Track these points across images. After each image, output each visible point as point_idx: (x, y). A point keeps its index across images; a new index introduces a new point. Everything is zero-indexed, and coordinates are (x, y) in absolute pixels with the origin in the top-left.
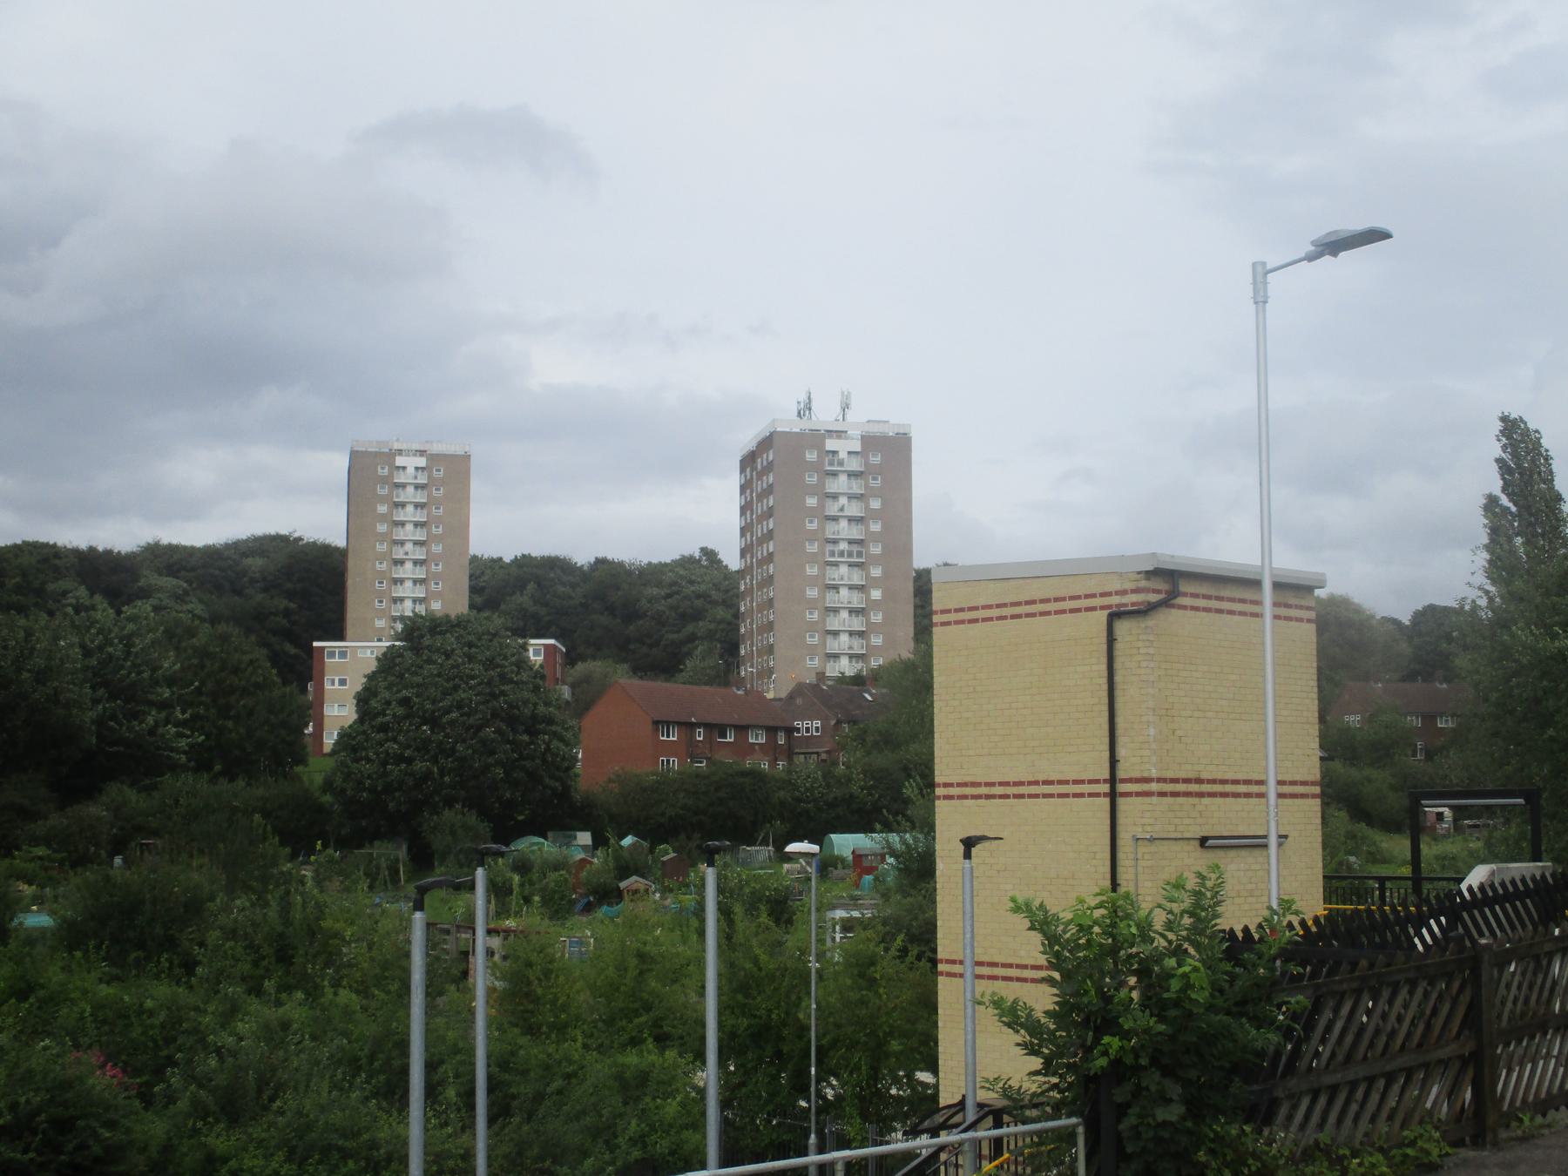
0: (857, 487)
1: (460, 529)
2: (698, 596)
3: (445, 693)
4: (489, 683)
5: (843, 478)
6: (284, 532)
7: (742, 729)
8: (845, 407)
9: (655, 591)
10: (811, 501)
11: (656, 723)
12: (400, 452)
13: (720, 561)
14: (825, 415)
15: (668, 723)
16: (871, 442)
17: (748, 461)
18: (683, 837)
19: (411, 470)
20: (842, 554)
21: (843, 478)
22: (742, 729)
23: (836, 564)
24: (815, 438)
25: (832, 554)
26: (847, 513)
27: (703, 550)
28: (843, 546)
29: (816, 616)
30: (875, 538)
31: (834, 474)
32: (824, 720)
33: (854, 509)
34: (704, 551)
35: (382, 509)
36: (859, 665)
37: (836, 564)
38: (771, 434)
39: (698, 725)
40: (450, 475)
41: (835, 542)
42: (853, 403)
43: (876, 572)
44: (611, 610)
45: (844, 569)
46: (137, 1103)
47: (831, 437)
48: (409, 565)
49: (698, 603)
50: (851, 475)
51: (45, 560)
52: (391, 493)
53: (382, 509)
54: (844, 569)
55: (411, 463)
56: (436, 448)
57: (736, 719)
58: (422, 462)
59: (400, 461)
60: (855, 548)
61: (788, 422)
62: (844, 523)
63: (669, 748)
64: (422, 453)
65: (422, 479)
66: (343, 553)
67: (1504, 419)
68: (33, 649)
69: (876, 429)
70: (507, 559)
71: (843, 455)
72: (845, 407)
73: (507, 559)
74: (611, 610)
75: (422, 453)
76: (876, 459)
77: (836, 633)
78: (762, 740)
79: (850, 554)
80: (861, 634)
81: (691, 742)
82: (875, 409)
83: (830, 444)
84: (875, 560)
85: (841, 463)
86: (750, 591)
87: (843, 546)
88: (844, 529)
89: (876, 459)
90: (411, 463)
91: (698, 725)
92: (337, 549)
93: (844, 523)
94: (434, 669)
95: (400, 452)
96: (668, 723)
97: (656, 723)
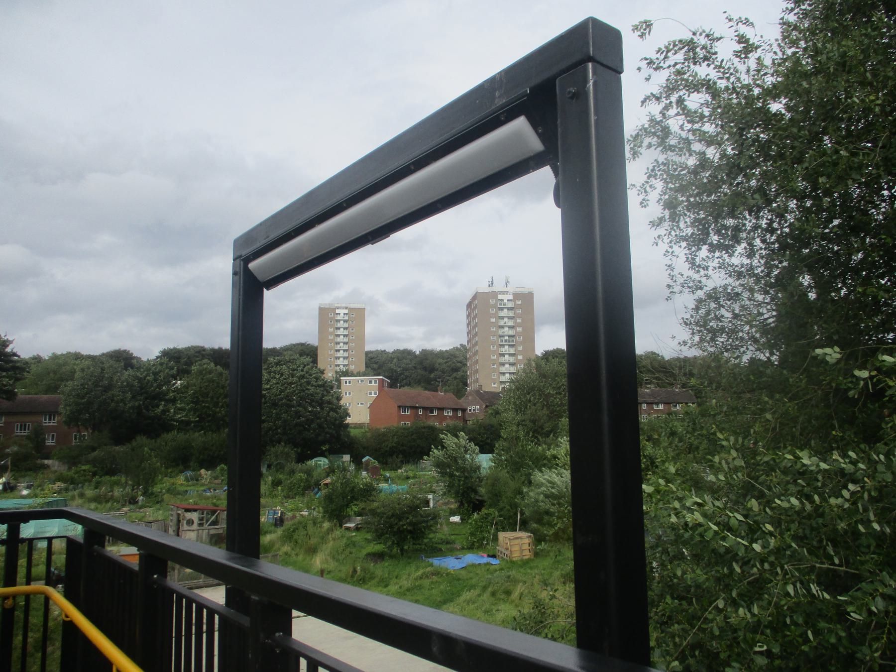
0: (511, 314)
1: (361, 338)
3: (281, 391)
4: (301, 385)
5: (506, 310)
6: (303, 342)
7: (441, 409)
8: (507, 283)
9: (441, 361)
10: (493, 320)
11: (399, 407)
12: (338, 308)
15: (405, 407)
16: (516, 296)
18: (394, 457)
19: (342, 315)
21: (506, 310)
22: (441, 409)
24: (494, 295)
28: (506, 338)
31: (502, 309)
32: (481, 405)
33: (511, 323)
35: (331, 330)
39: (420, 408)
40: (357, 316)
42: (510, 280)
43: (520, 348)
44: (425, 369)
45: (507, 347)
48: (341, 352)
50: (509, 309)
51: (199, 352)
52: (498, 368)
53: (331, 330)
54: (507, 347)
55: (342, 312)
56: (352, 306)
57: (438, 405)
58: (346, 311)
59: (337, 311)
61: (484, 288)
62: (506, 329)
63: (406, 418)
64: (346, 308)
65: (346, 318)
66: (316, 348)
67: (633, 30)
68: (104, 376)
69: (518, 290)
71: (505, 301)
72: (507, 283)
74: (425, 369)
75: (346, 308)
76: (519, 302)
78: (450, 414)
81: (417, 415)
83: (500, 297)
85: (504, 304)
86: (470, 357)
87: (506, 338)
89: (519, 302)
90: (342, 312)
91: (420, 408)
92: (312, 347)
93: (506, 329)
94: (274, 381)
95: (338, 308)
96: (405, 407)
97: (399, 407)
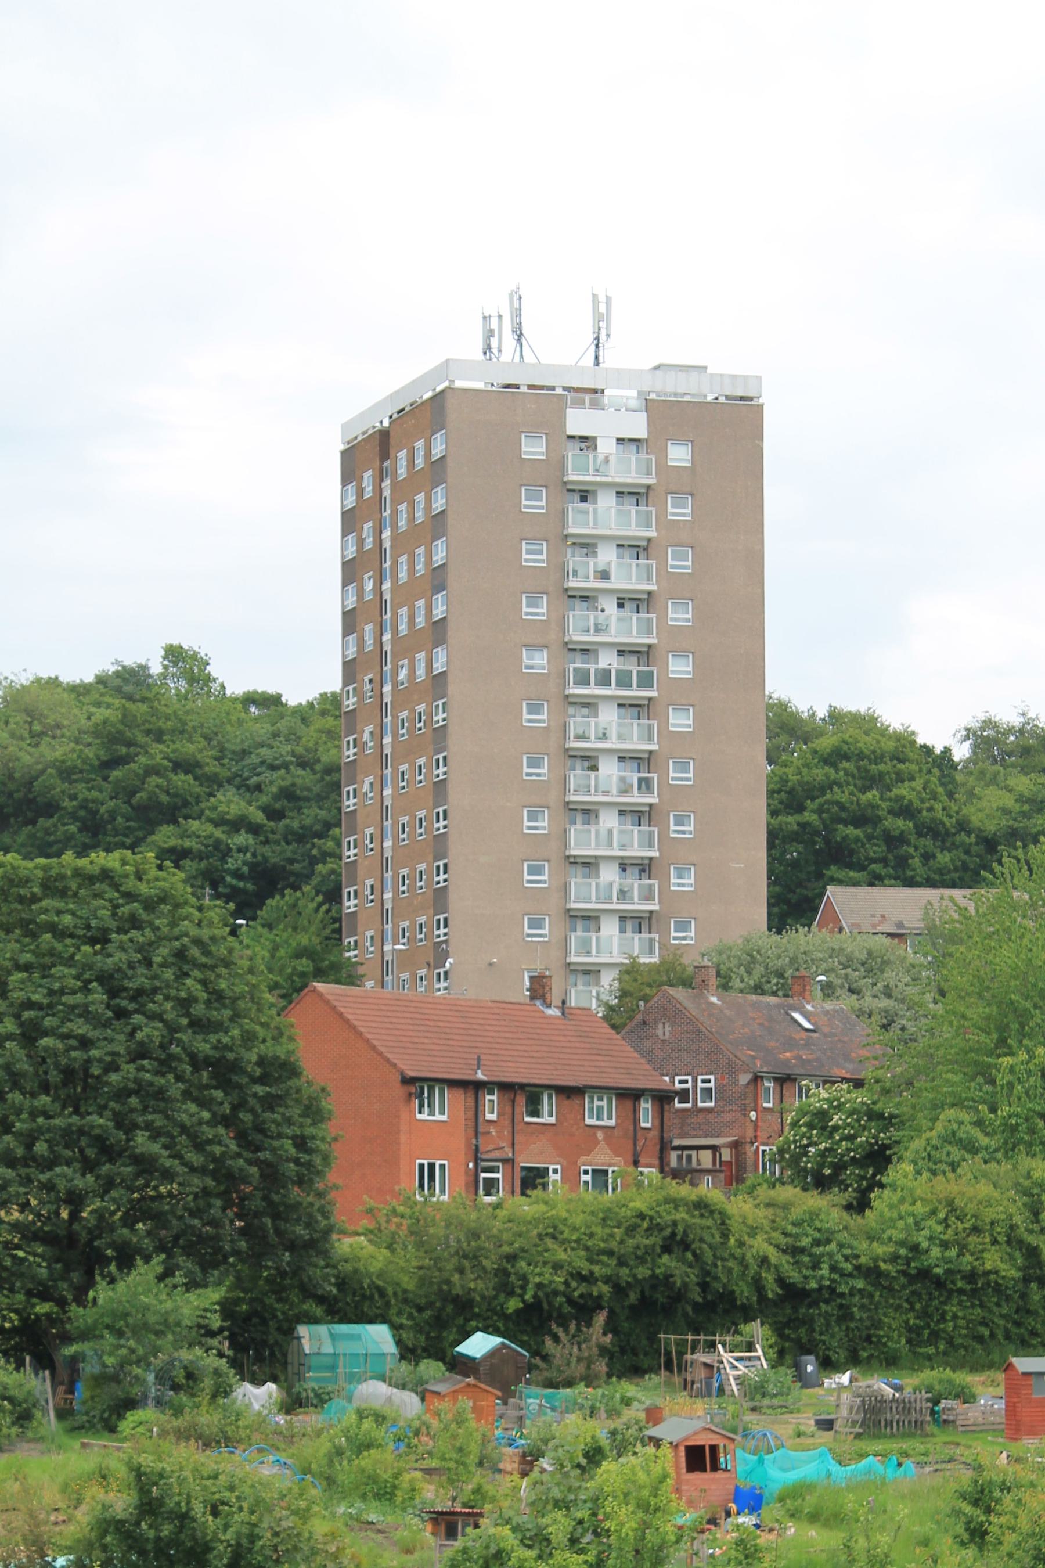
0: (630, 523)
2: (180, 765)
13: (209, 679)
14: (555, 350)
16: (671, 415)
17: (370, 455)
20: (604, 678)
23: (589, 705)
24: (541, 404)
25: (583, 679)
26: (617, 583)
27: (174, 654)
28: (607, 660)
29: (543, 823)
30: (679, 641)
33: (628, 576)
34: (174, 654)
36: (636, 942)
37: (589, 705)
38: (439, 398)
41: (587, 651)
45: (608, 716)
46: (443, 1224)
47: (579, 404)
49: (182, 781)
60: (632, 666)
69: (672, 386)
70: (920, 740)
73: (304, 703)
77: (590, 865)
79: (624, 680)
80: (645, 868)
82: (675, 330)
83: (578, 421)
84: (680, 694)
87: (607, 660)
88: (622, 627)
89: (679, 455)
